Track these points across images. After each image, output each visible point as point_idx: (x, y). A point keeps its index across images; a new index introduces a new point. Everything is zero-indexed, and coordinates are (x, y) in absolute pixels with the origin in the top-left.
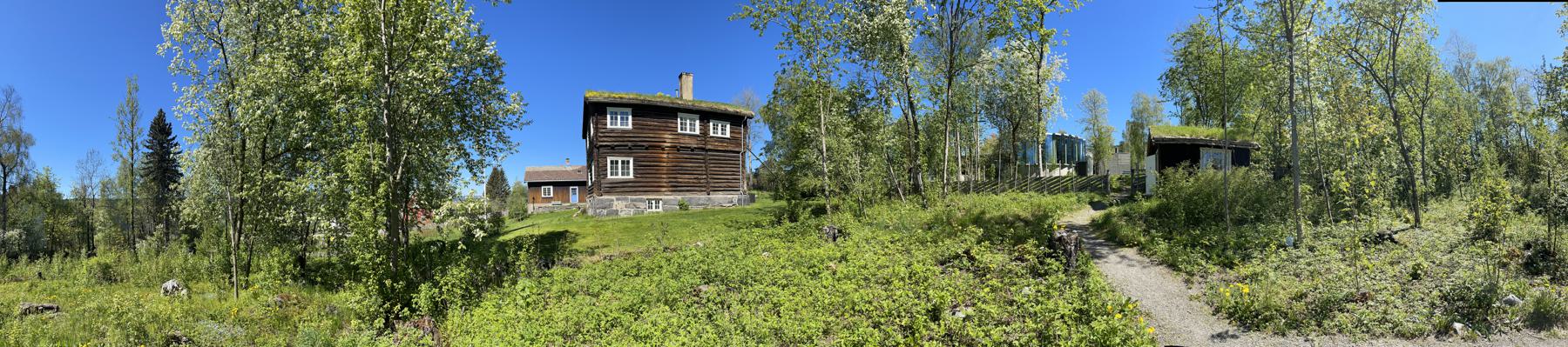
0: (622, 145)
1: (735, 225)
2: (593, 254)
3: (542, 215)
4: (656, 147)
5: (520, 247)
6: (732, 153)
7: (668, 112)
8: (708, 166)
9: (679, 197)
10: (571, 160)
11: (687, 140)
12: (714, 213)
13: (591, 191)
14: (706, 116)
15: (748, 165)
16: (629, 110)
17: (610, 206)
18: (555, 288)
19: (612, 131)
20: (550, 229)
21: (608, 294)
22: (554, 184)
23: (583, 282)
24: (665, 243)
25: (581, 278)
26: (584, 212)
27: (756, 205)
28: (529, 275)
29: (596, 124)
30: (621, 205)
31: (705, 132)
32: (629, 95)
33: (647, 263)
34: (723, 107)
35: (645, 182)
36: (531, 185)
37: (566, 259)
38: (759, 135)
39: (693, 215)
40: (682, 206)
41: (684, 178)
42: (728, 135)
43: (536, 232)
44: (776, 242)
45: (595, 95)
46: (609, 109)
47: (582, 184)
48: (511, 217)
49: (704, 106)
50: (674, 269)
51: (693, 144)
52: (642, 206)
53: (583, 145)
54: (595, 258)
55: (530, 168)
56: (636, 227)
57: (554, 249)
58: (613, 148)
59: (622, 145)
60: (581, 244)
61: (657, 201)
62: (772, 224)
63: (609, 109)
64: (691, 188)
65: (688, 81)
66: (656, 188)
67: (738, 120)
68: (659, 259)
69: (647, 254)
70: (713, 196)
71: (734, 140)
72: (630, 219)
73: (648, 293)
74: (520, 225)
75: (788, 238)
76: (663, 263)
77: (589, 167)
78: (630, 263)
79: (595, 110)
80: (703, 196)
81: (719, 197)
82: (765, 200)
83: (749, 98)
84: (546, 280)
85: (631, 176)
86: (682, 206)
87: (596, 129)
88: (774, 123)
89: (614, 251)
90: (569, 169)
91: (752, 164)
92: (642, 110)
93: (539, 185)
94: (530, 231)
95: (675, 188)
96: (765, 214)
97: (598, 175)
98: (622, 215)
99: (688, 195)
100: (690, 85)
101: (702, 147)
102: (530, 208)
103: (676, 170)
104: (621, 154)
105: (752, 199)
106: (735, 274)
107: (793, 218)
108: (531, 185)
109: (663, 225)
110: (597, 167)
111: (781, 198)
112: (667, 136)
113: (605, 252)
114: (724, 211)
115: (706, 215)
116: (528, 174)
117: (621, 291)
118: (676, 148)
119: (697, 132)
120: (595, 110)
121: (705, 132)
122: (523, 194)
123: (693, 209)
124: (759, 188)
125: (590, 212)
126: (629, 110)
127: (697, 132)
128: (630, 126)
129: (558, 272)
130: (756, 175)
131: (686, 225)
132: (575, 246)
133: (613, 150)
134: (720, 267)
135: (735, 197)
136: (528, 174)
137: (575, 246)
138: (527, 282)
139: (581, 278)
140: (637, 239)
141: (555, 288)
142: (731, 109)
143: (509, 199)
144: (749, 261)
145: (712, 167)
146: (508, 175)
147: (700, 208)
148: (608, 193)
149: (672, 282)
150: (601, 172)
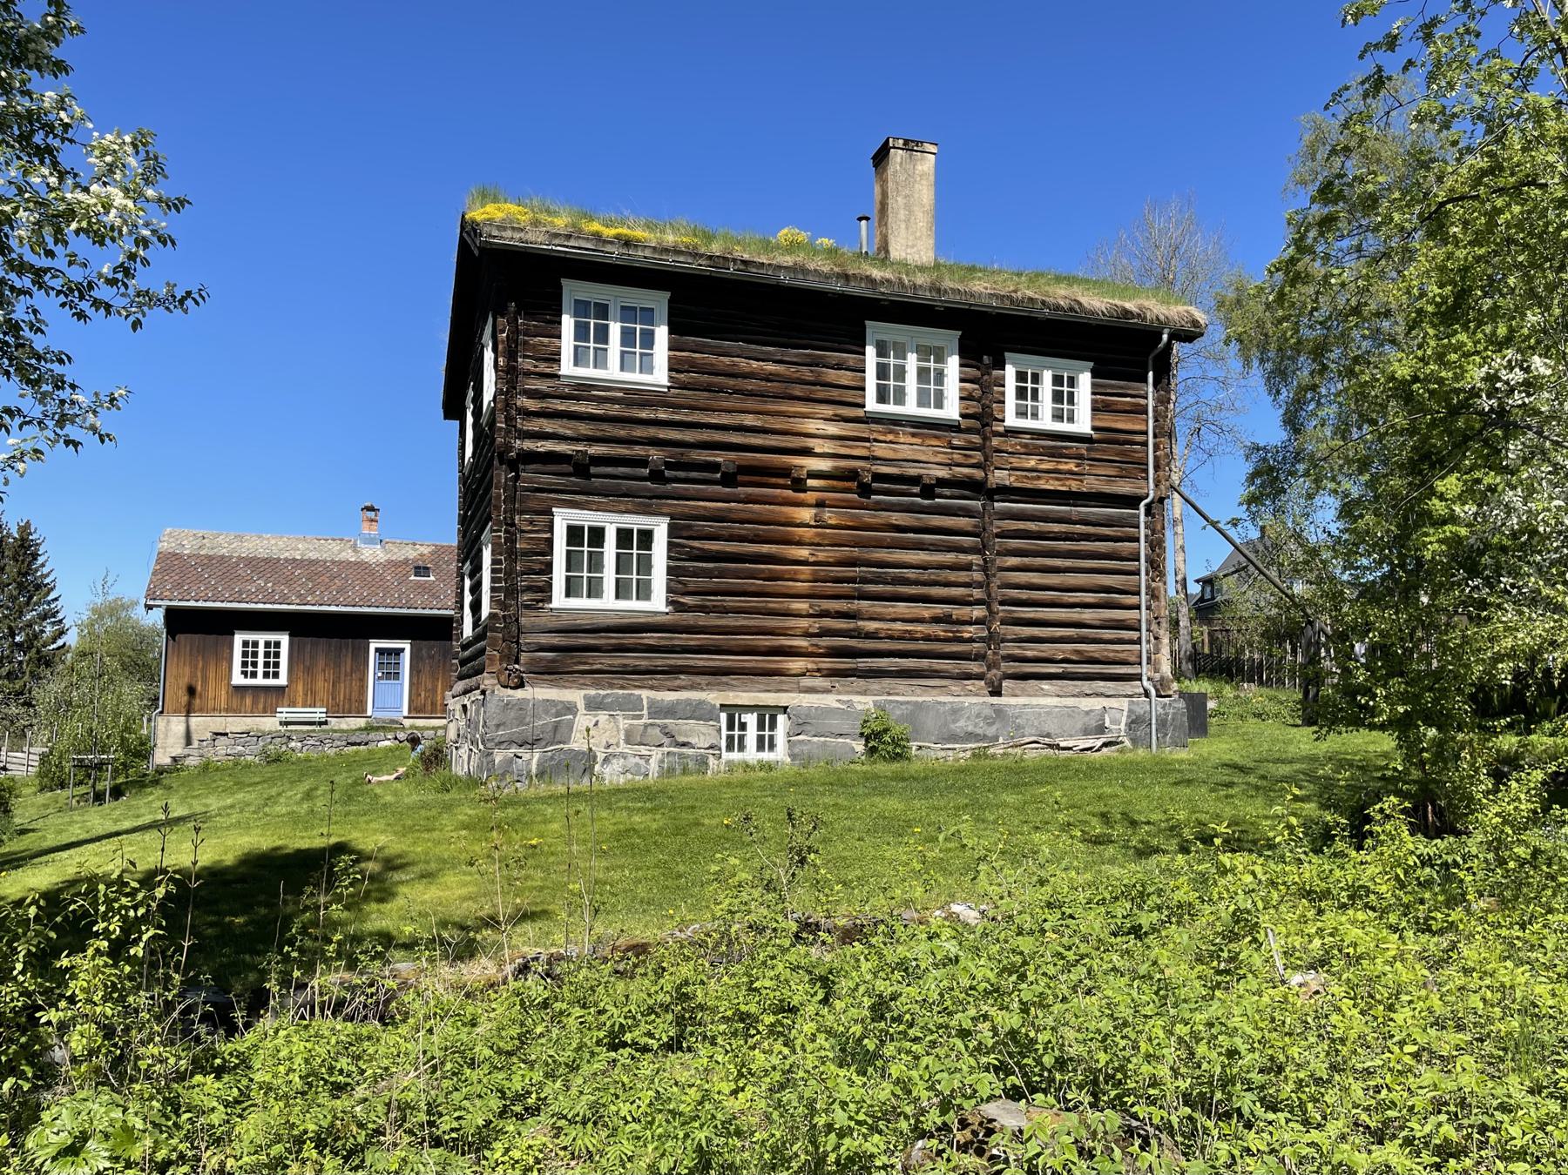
0: (622, 457)
1: (1113, 830)
2: (466, 951)
3: (234, 773)
4: (771, 473)
5: (76, 933)
6: (1106, 503)
7: (825, 319)
8: (1003, 561)
9: (864, 701)
10: (388, 525)
11: (906, 447)
12: (1018, 776)
13: (472, 667)
14: (990, 335)
15: (1172, 560)
16: (658, 301)
17: (559, 732)
18: (251, 1128)
19: (583, 390)
20: (260, 840)
21: (533, 1135)
22: (301, 625)
23: (411, 1084)
24: (801, 902)
25: (400, 1063)
26: (436, 758)
27: (1216, 748)
28: (117, 1071)
29: (510, 352)
30: (606, 730)
31: (981, 413)
32: (659, 234)
33: (718, 991)
34: (1060, 294)
35: (715, 635)
36: (179, 621)
37: (328, 980)
38: (1225, 411)
39: (928, 783)
40: (878, 740)
41: (887, 619)
42: (1083, 424)
43: (183, 853)
44: (1355, 928)
45: (510, 217)
46: (573, 290)
47: (430, 630)
48: (51, 778)
49: (982, 288)
50: (849, 1014)
51: (932, 460)
52: (700, 735)
53: (444, 449)
54: (479, 970)
55: (185, 539)
56: (673, 826)
57: (268, 935)
58: (581, 467)
59: (622, 457)
60: (409, 907)
61: (768, 717)
62: (1321, 839)
63: (573, 290)
64: (918, 660)
65: (916, 180)
66: (760, 658)
67: (1126, 352)
68: (783, 976)
69: (723, 950)
70: (1016, 699)
71: (1110, 444)
72: (647, 795)
73: (731, 1129)
74: (98, 819)
75: (1431, 901)
76: (799, 990)
77: (469, 552)
78: (639, 990)
79: (505, 288)
80: (971, 700)
81: (1042, 705)
82: (1261, 726)
83: (1189, 248)
84: (207, 1090)
85: (658, 602)
86: (878, 740)
87: (509, 375)
88: (1294, 346)
89: (569, 937)
90: (372, 554)
91: (1194, 554)
92: (713, 305)
93: (221, 624)
94: (146, 853)
95: (849, 659)
96: (1269, 788)
97: (507, 591)
98: (611, 774)
99: (907, 695)
100: (925, 193)
101: (972, 486)
102: (169, 737)
103: (856, 577)
104: (616, 497)
105: (1198, 720)
106: (1160, 1066)
107: (1437, 813)
108: (179, 621)
109: (793, 816)
110: (507, 551)
111: (1359, 718)
112: (819, 426)
113: (525, 942)
114: (1061, 769)
115: (989, 783)
116: (170, 564)
117: (595, 1117)
118: (855, 482)
119: (951, 410)
120: (505, 288)
121: (981, 413)
122: (138, 665)
123: (929, 753)
124: (1216, 663)
125: (463, 762)
126: (658, 301)
127: (951, 410)
128: (659, 376)
129: (278, 1044)
130: (1205, 609)
131: (898, 828)
132: (379, 918)
133: (583, 477)
134: (1074, 1027)
135: (1114, 706)
136: (170, 564)
137: (379, 918)
138: (101, 1110)
139: (400, 1063)
140: (674, 887)
141: (251, 1128)
142: (1097, 302)
143: (49, 690)
144: (1240, 1009)
145: (1014, 573)
146: (54, 562)
147: (961, 753)
148: (551, 672)
149: (846, 1083)
150: (525, 575)
